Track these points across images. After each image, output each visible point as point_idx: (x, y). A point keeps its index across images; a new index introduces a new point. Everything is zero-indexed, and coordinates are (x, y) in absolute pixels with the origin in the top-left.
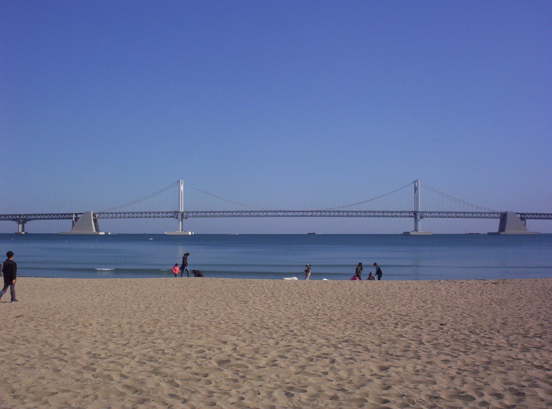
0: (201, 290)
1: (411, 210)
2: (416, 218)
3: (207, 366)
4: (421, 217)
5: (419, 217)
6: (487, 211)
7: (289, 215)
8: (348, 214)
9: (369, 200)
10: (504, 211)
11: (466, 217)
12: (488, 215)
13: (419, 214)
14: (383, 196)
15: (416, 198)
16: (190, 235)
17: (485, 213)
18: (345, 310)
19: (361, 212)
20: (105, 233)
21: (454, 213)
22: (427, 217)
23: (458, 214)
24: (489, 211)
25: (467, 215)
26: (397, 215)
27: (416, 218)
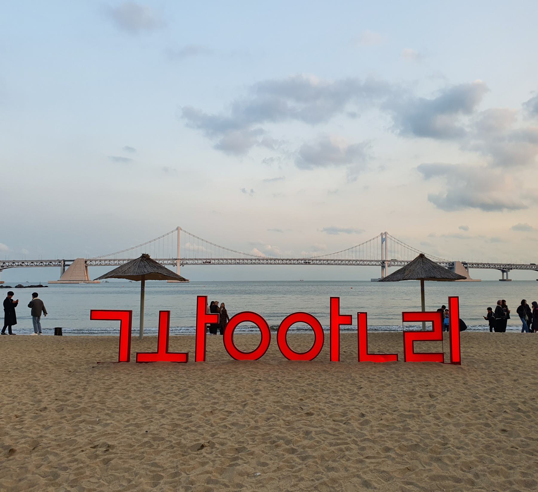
5: (386, 265)
10: (452, 260)
19: (294, 260)
26: (272, 262)
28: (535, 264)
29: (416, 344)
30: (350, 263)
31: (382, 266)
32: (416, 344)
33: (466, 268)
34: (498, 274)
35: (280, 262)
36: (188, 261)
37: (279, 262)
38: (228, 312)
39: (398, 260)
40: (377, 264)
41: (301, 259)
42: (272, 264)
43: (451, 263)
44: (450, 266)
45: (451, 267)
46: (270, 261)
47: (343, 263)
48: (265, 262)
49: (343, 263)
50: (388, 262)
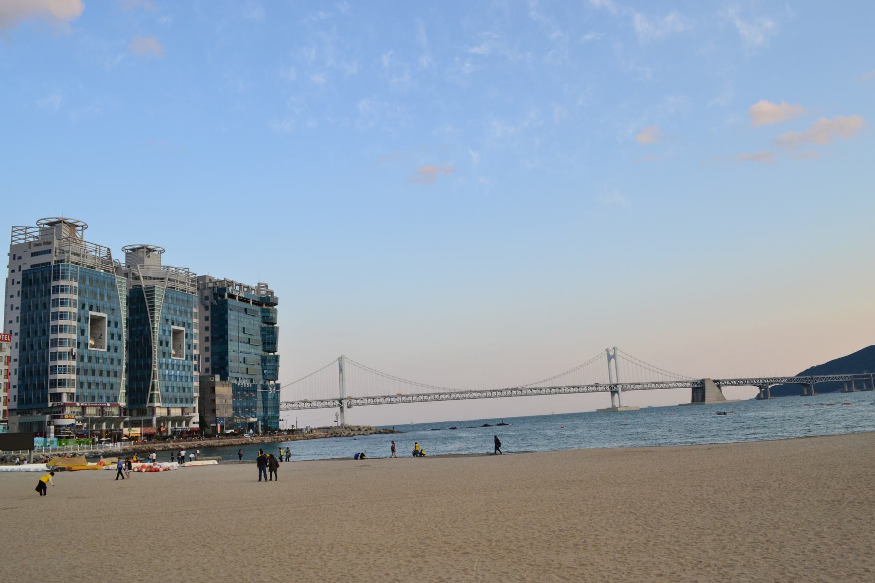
0: (434, 575)
1: (336, 398)
2: (342, 408)
3: (507, 577)
4: (349, 407)
5: (345, 406)
6: (446, 391)
7: (475, 396)
8: (540, 391)
9: (297, 381)
10: (699, 377)
11: (410, 402)
12: (676, 385)
13: (345, 402)
14: (315, 373)
15: (342, 380)
16: (217, 374)
17: (445, 394)
18: (636, 550)
19: (316, 401)
20: (218, 405)
21: (415, 395)
22: (357, 405)
23: (662, 385)
24: (448, 391)
25: (453, 396)
26: (317, 405)
27: (342, 408)
28: (628, 407)
29: (219, 376)
30: (408, 400)
31: (611, 392)
32: (219, 376)
33: (719, 386)
34: (613, 360)
35: (319, 404)
36: (490, 394)
37: (329, 404)
38: (21, 286)
39: (403, 394)
40: (480, 395)
41: (328, 400)
42: (294, 409)
43: (699, 382)
44: (698, 385)
45: (699, 386)
46: (314, 404)
47: (408, 400)
48: (319, 404)
49: (483, 395)
50: (621, 386)
